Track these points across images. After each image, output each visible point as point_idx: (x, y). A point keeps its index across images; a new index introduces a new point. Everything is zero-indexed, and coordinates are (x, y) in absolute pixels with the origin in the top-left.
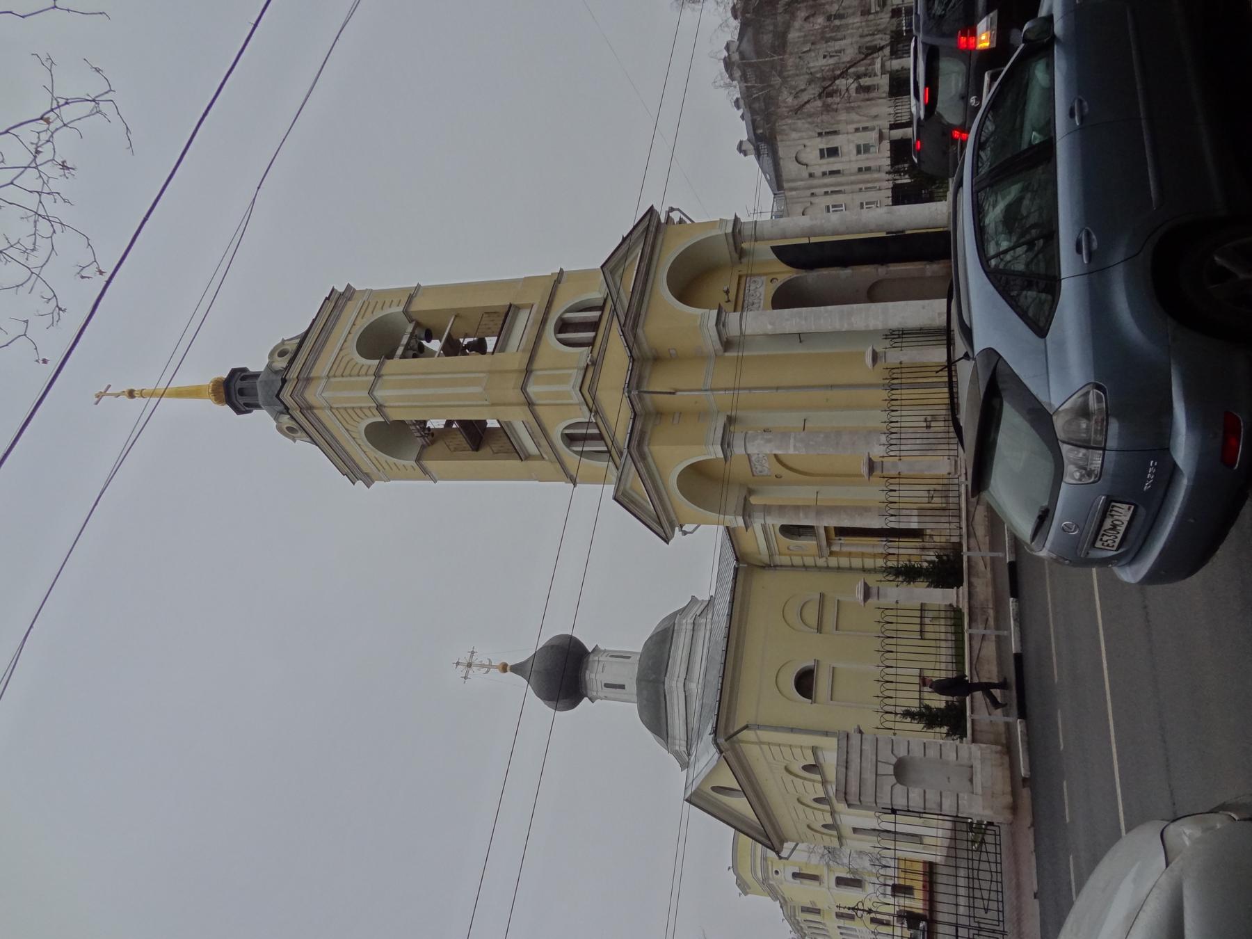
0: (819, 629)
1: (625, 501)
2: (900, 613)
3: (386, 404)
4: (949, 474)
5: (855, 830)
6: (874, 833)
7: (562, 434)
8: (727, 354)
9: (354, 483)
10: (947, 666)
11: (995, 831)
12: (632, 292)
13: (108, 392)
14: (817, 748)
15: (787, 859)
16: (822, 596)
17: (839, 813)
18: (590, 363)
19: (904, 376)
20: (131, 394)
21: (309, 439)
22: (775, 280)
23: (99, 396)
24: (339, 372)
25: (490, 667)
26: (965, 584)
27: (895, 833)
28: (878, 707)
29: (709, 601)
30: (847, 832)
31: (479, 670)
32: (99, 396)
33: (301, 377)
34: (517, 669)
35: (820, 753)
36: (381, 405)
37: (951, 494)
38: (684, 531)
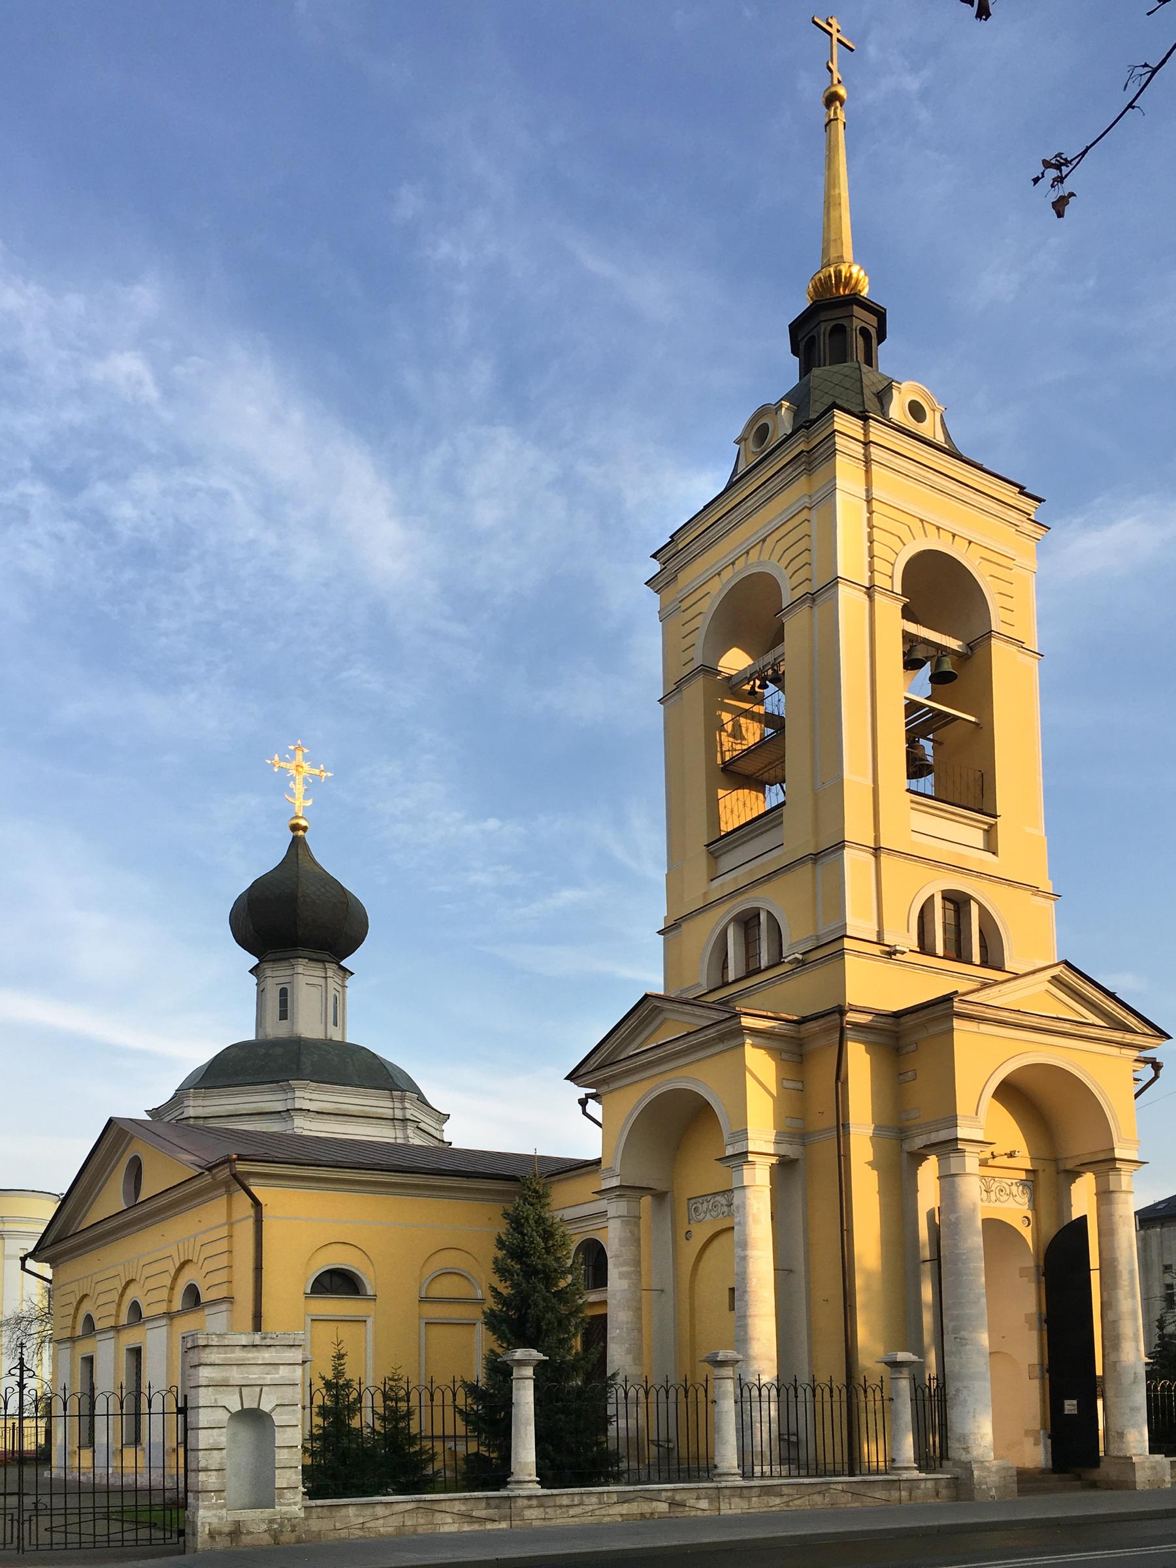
0: (423, 1300)
1: (644, 1011)
3: (815, 609)
5: (89, 1361)
6: (88, 1387)
7: (758, 909)
8: (905, 1155)
9: (654, 556)
14: (232, 1303)
15: (23, 1268)
17: (116, 1338)
21: (742, 469)
26: (923, 1475)
27: (92, 1416)
28: (369, 1383)
29: (443, 1141)
30: (84, 1348)
35: (224, 1307)
36: (814, 600)
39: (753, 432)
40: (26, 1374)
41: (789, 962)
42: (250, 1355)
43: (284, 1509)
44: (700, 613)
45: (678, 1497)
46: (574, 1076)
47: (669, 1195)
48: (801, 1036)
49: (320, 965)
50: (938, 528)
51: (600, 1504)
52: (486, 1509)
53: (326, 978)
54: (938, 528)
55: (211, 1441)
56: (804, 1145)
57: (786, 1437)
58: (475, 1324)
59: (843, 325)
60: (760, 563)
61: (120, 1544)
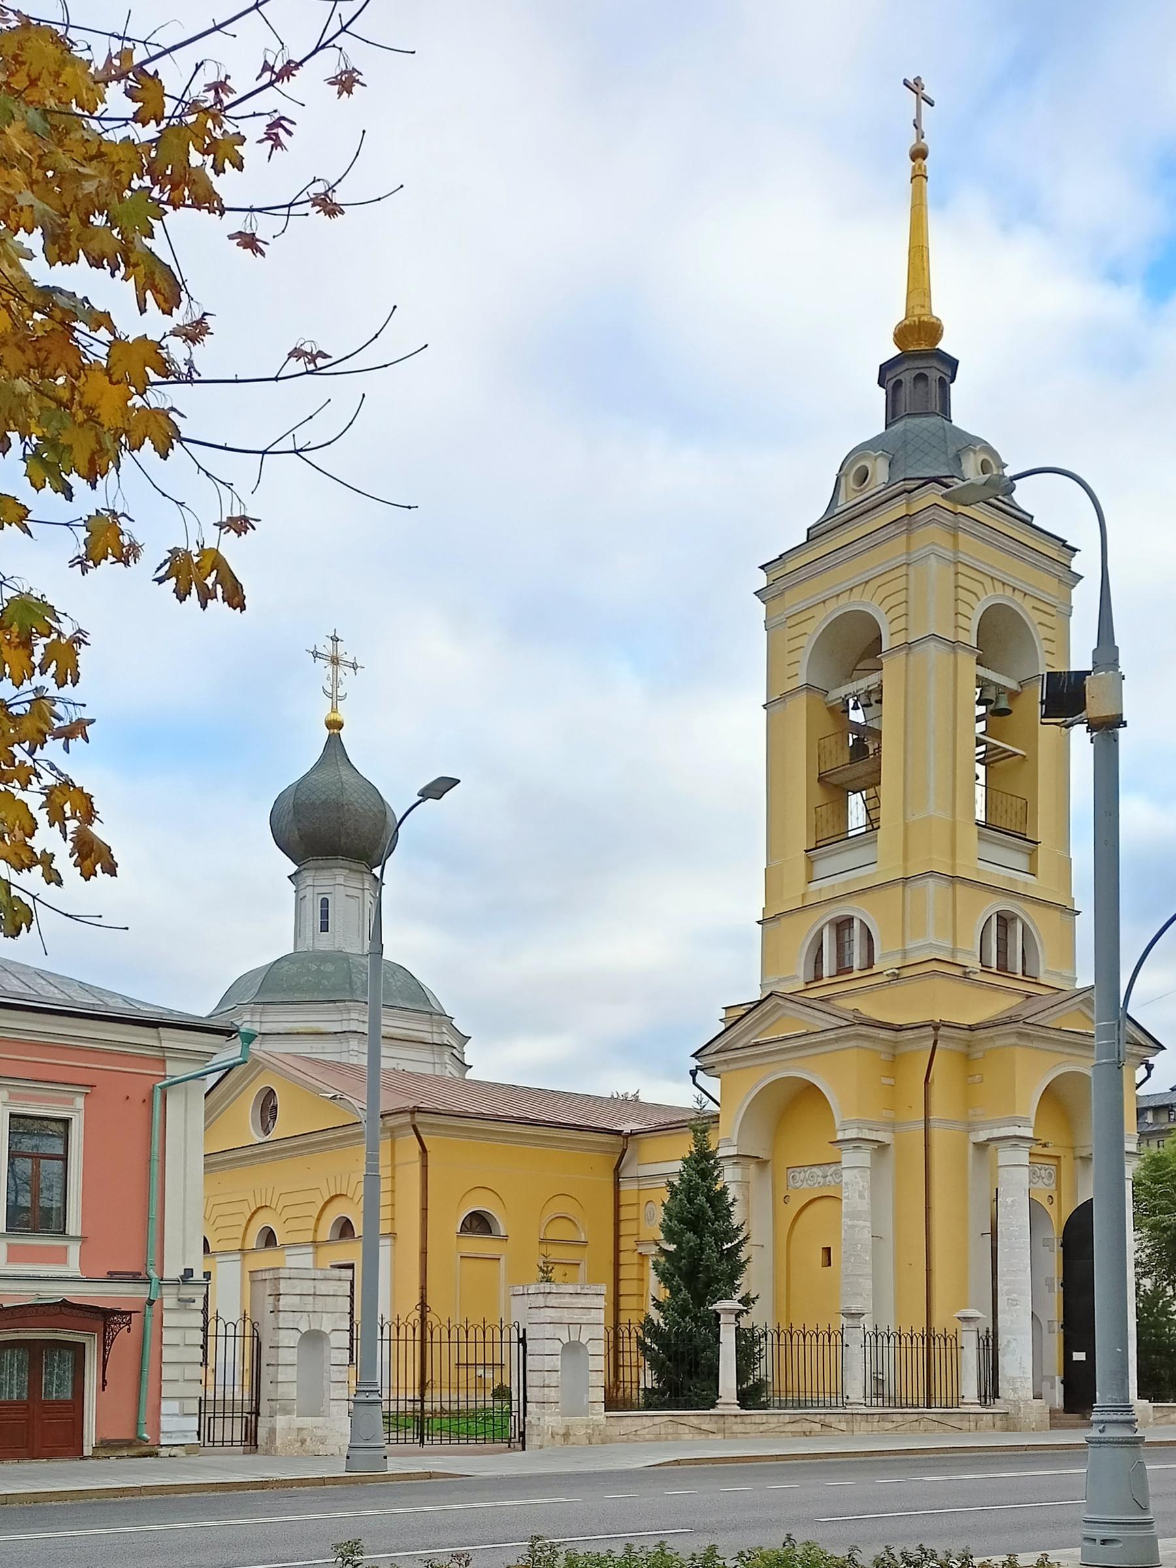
0: (543, 1241)
2: (840, 1348)
3: (911, 658)
4: (848, 1397)
10: (182, 1407)
11: (515, 1438)
13: (923, 101)
14: (394, 1238)
18: (968, 970)
19: (948, 1351)
20: (919, 154)
22: (1051, 1201)
23: (915, 86)
24: (962, 581)
25: (335, 698)
31: (328, 678)
32: (915, 86)
33: (961, 519)
34: (334, 746)
37: (880, 1400)
38: (697, 1073)
39: (854, 470)
41: (887, 975)
42: (574, 1301)
43: (595, 1417)
44: (805, 634)
45: (828, 1419)
46: (699, 1055)
47: (770, 1163)
48: (898, 1040)
49: (358, 876)
50: (1004, 584)
51: (779, 1423)
52: (708, 1424)
53: (363, 889)
54: (1004, 584)
55: (552, 1365)
56: (893, 1132)
57: (876, 1375)
58: (579, 1264)
59: (925, 375)
60: (863, 604)
61: (230, 1444)
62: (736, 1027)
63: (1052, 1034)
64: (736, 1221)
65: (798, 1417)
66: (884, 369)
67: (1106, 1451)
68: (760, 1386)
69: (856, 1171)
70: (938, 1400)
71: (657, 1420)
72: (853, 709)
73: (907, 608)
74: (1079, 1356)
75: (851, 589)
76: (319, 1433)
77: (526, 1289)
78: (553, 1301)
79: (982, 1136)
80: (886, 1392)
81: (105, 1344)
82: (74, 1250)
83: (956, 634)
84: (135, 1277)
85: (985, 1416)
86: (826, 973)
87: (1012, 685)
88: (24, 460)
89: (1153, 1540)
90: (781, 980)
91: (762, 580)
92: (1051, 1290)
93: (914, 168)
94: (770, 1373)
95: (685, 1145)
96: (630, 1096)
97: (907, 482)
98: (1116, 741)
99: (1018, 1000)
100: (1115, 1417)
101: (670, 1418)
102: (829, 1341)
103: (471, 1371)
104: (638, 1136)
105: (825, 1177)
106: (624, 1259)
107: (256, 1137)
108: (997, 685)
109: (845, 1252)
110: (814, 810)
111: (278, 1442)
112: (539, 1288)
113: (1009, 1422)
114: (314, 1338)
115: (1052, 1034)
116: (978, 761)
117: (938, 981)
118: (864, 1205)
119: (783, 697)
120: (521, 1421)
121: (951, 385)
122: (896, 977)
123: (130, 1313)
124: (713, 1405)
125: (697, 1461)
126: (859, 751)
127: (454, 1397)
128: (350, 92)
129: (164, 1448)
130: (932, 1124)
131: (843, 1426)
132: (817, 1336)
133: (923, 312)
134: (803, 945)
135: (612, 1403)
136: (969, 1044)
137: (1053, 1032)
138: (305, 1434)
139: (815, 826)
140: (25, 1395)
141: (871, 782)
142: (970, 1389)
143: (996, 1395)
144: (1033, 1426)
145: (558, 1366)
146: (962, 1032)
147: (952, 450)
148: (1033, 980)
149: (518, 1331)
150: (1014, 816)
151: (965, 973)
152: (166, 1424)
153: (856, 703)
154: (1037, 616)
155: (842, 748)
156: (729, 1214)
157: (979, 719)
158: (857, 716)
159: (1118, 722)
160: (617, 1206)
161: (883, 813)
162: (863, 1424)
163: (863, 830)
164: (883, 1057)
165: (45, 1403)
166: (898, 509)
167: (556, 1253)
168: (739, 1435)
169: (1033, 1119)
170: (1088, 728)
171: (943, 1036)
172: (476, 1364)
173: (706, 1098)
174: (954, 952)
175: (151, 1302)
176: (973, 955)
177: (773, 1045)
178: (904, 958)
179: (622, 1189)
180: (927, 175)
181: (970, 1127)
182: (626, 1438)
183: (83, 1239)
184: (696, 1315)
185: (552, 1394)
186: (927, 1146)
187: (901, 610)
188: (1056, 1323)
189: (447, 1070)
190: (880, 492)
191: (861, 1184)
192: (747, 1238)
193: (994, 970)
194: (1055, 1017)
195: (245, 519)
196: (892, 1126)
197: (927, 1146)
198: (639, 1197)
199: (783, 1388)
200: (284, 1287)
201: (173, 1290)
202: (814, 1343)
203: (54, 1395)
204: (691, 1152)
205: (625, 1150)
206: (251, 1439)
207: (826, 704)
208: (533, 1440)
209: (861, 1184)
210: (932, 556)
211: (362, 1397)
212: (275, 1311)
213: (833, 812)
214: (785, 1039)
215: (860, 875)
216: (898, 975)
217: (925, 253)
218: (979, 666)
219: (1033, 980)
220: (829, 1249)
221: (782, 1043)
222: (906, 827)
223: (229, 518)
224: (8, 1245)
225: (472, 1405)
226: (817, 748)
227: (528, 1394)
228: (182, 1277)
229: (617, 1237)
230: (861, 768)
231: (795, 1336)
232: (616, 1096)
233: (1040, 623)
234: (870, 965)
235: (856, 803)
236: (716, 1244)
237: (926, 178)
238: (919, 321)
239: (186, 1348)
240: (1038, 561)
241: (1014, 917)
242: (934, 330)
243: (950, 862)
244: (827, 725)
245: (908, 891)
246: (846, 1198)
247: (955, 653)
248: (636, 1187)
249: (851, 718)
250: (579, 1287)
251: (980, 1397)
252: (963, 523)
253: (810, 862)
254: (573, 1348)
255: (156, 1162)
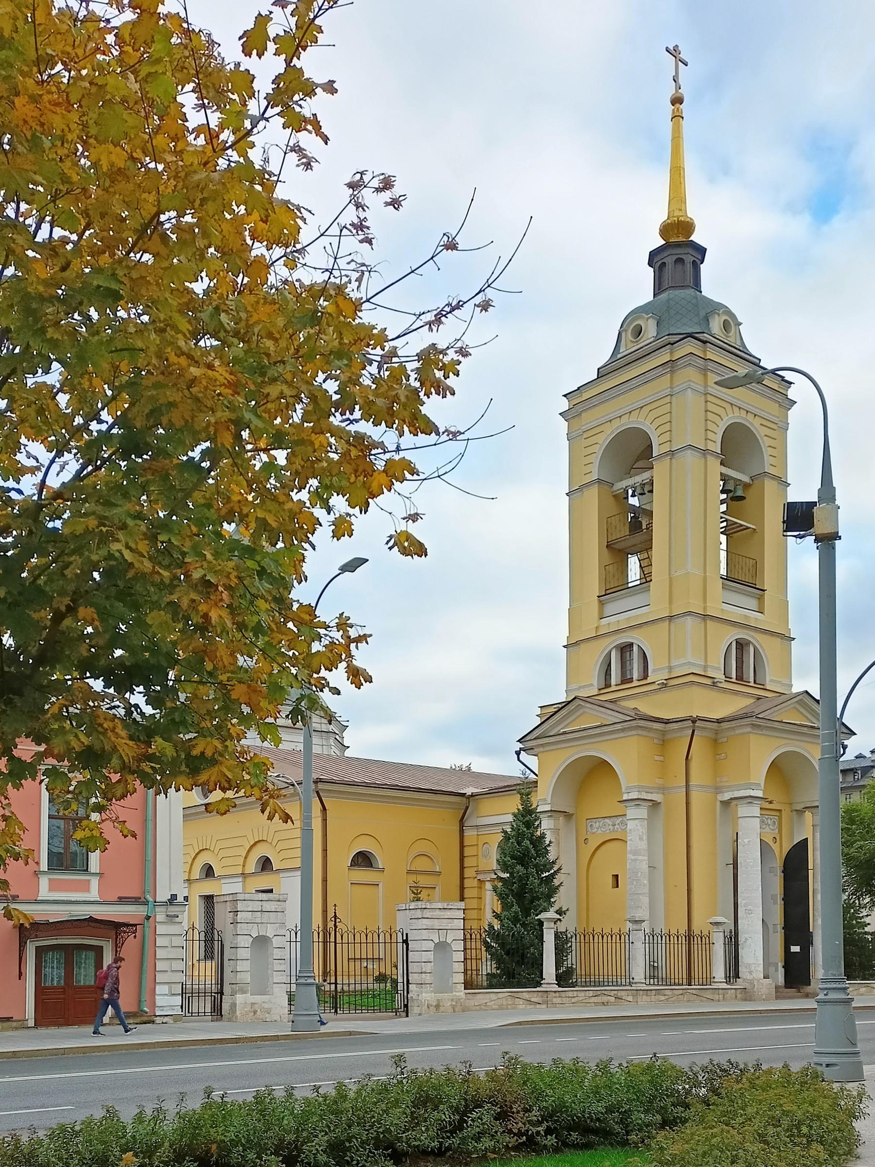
0: (409, 872)
3: (674, 461)
4: (633, 979)
10: (170, 990)
12: (781, 722)
13: (680, 62)
16: (439, 873)
18: (716, 681)
20: (677, 101)
24: (710, 407)
32: (674, 52)
40: (338, 920)
42: (442, 913)
43: (457, 994)
45: (620, 994)
47: (574, 816)
50: (740, 408)
60: (639, 423)
62: (550, 721)
63: (776, 725)
64: (551, 857)
65: (599, 993)
66: (653, 255)
67: (829, 1008)
68: (570, 972)
69: (637, 821)
70: (696, 980)
71: (500, 995)
72: (631, 496)
73: (671, 426)
74: (795, 949)
75: (630, 412)
76: (266, 1006)
77: (407, 905)
78: (427, 914)
79: (727, 796)
80: (660, 976)
81: (116, 946)
82: (95, 883)
83: (706, 445)
84: (136, 901)
85: (729, 991)
86: (613, 682)
87: (746, 479)
88: (309, 493)
89: (859, 1065)
90: (580, 687)
91: (565, 405)
92: (775, 903)
93: (674, 110)
94: (574, 962)
95: (514, 804)
96: (464, 767)
97: (669, 337)
98: (834, 548)
99: (752, 701)
100: (835, 986)
101: (510, 994)
102: (620, 940)
103: (358, 963)
104: (477, 797)
105: (614, 825)
106: (467, 883)
107: (198, 800)
108: (736, 480)
109: (630, 878)
110: (603, 568)
111: (238, 1013)
112: (417, 905)
113: (747, 995)
114: (261, 942)
115: (776, 725)
116: (722, 533)
117: (695, 689)
118: (643, 845)
119: (582, 488)
120: (405, 997)
121: (701, 265)
122: (664, 686)
123: (135, 925)
124: (539, 984)
125: (532, 1022)
126: (635, 526)
127: (346, 981)
128: (486, 311)
129: (158, 1018)
130: (691, 788)
131: (630, 998)
132: (612, 936)
133: (681, 214)
134: (597, 661)
135: (468, 985)
136: (717, 732)
137: (776, 723)
138: (256, 1007)
139: (605, 578)
140: (62, 982)
141: (647, 546)
142: (719, 972)
143: (737, 976)
144: (764, 997)
145: (432, 958)
146: (712, 724)
147: (702, 314)
148: (762, 687)
149: (403, 934)
150: (747, 572)
151: (714, 683)
152: (160, 1001)
153: (634, 492)
154: (764, 431)
155: (624, 525)
156: (547, 852)
157: (722, 502)
158: (634, 501)
159: (836, 536)
160: (462, 847)
161: (655, 569)
162: (644, 997)
163: (638, 582)
164: (656, 741)
165: (76, 987)
166: (664, 356)
167: (424, 881)
168: (557, 1005)
169: (763, 784)
170: (815, 540)
171: (698, 727)
172: (361, 959)
173: (528, 772)
174: (705, 667)
175: (148, 918)
176: (719, 669)
177: (576, 733)
178: (670, 672)
179: (465, 834)
180: (683, 116)
181: (718, 790)
182: (483, 1008)
183: (101, 874)
184: (524, 922)
185: (427, 978)
186: (688, 804)
187: (667, 427)
188: (779, 926)
189: (332, 750)
190: (651, 343)
191: (641, 830)
192: (560, 869)
193: (734, 680)
194: (777, 713)
195: (417, 514)
196: (663, 789)
197: (688, 804)
198: (477, 841)
199: (583, 973)
200: (240, 906)
201: (163, 909)
202: (610, 941)
203: (82, 982)
204: (518, 809)
205: (467, 808)
206: (217, 1011)
207: (612, 492)
208: (414, 1009)
209: (641, 830)
210: (689, 389)
211: (302, 981)
212: (235, 923)
213: (618, 569)
214: (585, 729)
215: (638, 613)
216: (666, 684)
217: (682, 172)
218: (722, 467)
219: (762, 687)
220: (617, 876)
221: (581, 732)
222: (671, 579)
223: (409, 515)
224: (50, 879)
225: (358, 987)
226: (606, 525)
227: (410, 978)
228: (169, 900)
229: (462, 868)
230: (638, 538)
231: (596, 937)
232: (454, 767)
233: (766, 436)
234: (646, 677)
235: (633, 563)
236: (537, 873)
237: (683, 118)
238: (678, 220)
239: (172, 949)
240: (766, 392)
241: (748, 643)
242: (688, 227)
243: (702, 604)
244: (613, 508)
245: (672, 625)
246: (630, 840)
247: (706, 458)
248: (476, 833)
249: (630, 502)
250: (445, 904)
251: (726, 977)
252: (711, 366)
253: (602, 604)
254: (442, 947)
255: (150, 822)
